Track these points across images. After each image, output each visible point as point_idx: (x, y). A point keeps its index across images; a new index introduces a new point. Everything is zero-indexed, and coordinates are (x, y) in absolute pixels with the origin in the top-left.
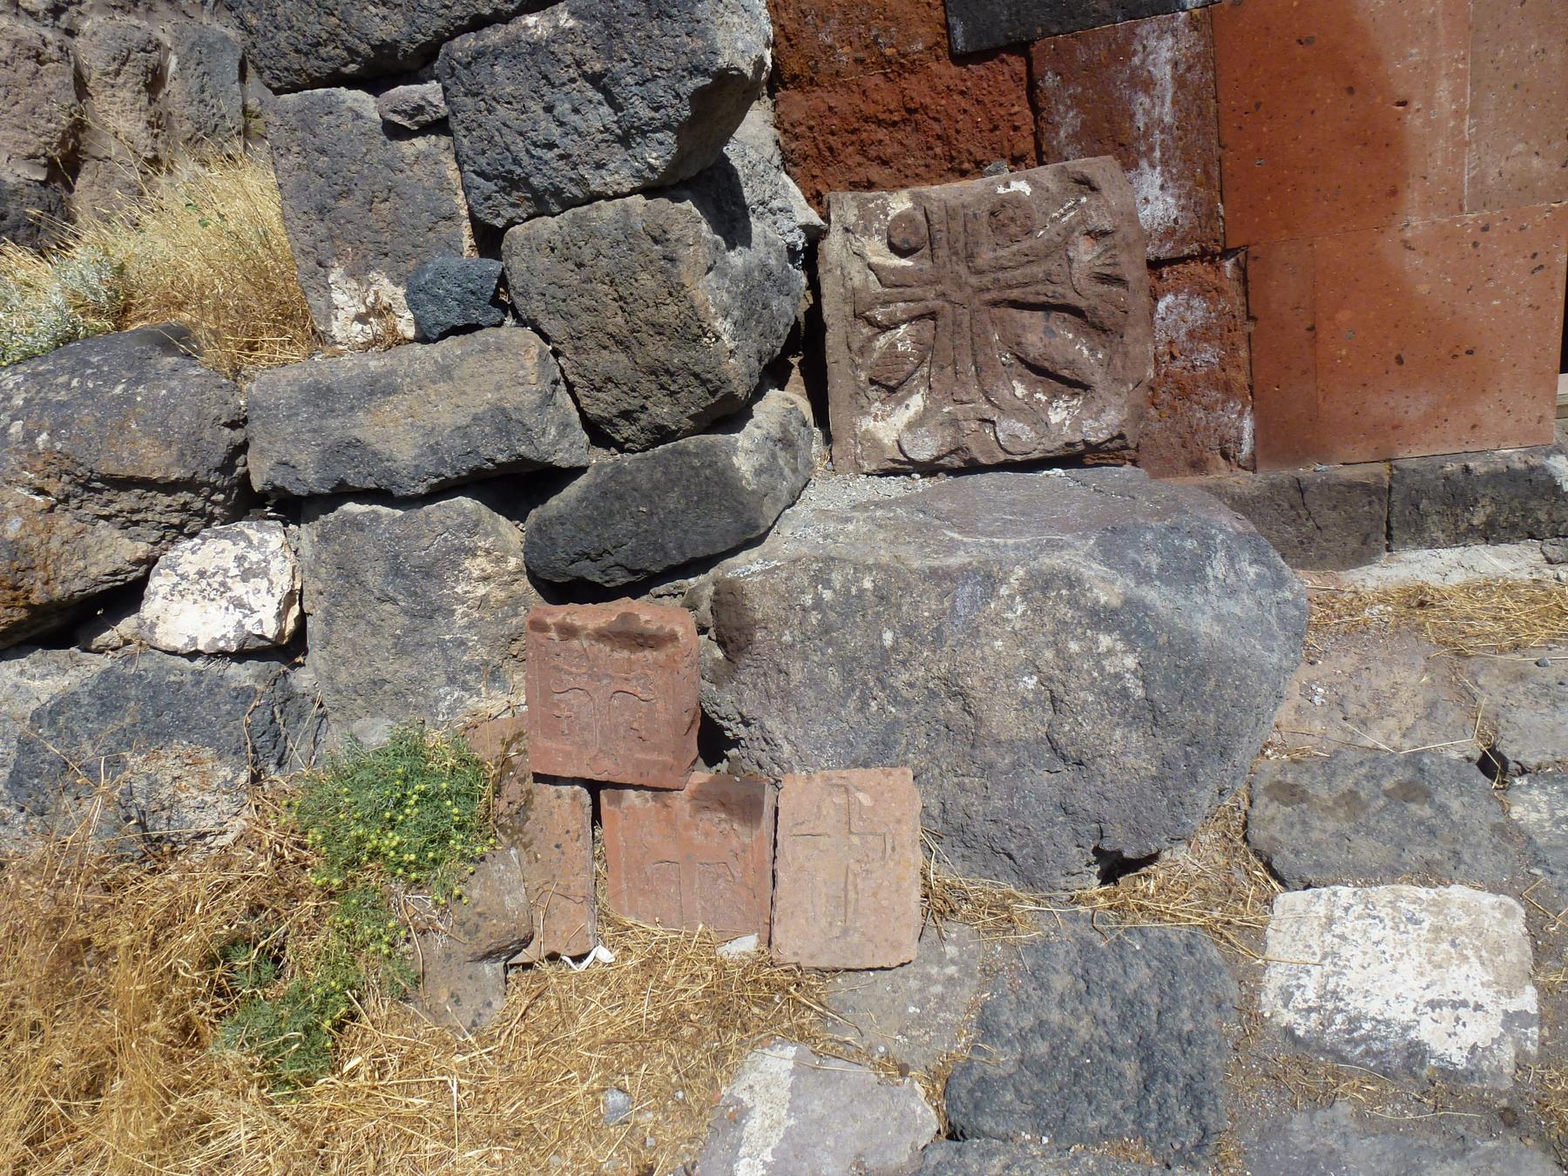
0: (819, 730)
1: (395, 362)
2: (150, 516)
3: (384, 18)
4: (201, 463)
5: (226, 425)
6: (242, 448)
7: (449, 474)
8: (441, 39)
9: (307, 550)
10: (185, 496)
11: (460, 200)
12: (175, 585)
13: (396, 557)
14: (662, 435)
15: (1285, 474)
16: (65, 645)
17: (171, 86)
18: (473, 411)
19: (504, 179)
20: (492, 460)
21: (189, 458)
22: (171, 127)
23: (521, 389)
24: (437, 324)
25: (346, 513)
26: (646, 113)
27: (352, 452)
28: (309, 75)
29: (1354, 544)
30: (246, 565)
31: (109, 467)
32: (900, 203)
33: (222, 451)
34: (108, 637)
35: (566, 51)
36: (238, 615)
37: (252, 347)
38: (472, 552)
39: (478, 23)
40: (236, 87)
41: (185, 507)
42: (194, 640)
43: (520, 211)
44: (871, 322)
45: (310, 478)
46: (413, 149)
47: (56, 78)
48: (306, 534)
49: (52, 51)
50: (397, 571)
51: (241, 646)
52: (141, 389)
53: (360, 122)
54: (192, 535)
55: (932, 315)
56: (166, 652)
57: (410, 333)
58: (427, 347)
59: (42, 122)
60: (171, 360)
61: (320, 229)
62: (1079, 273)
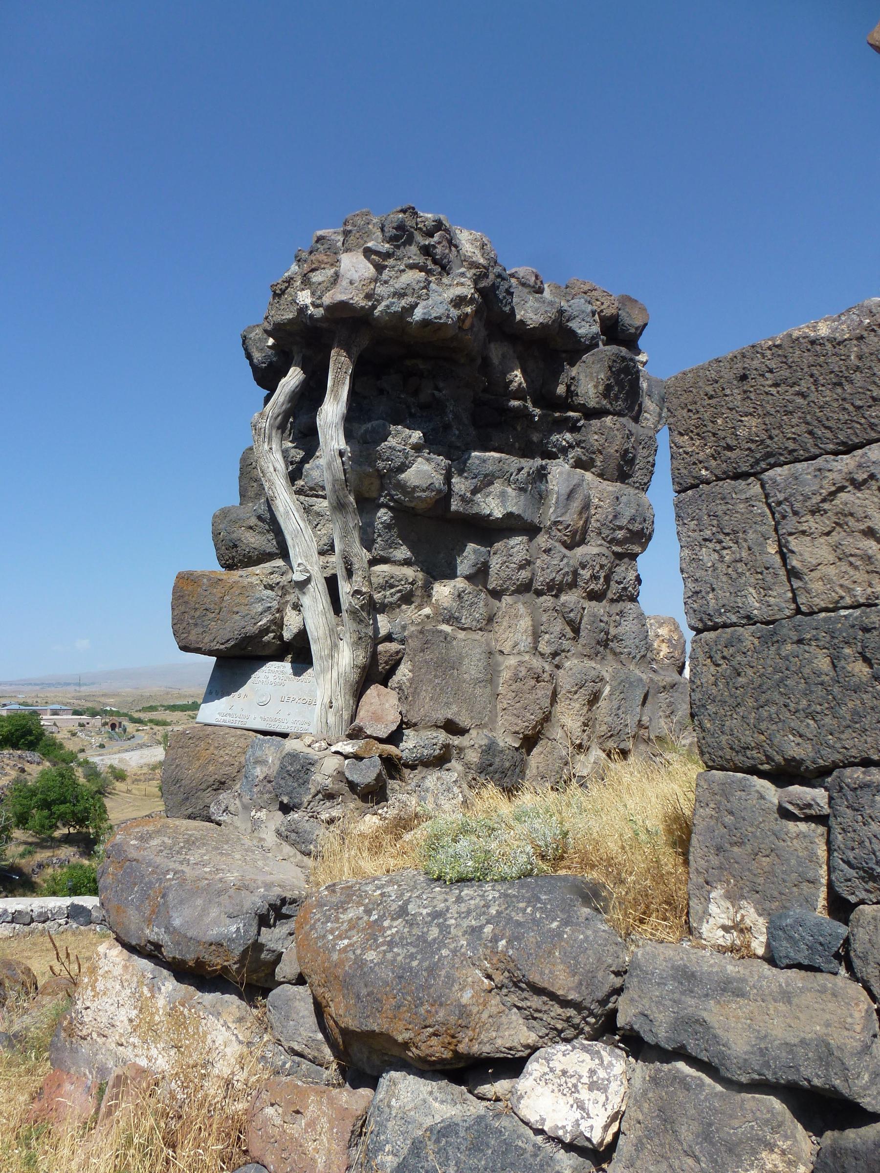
1: (747, 972)
2: (545, 1017)
3: (798, 744)
4: (590, 994)
5: (613, 972)
6: (618, 991)
7: (770, 1077)
8: (835, 766)
9: (637, 1082)
10: (571, 1012)
11: (823, 871)
12: (545, 1074)
13: (710, 1125)
16: (459, 1083)
17: (602, 703)
18: (802, 1035)
19: (865, 871)
20: (809, 1081)
21: (583, 988)
22: (594, 726)
23: (846, 1033)
24: (787, 957)
25: (678, 1070)
27: (698, 1028)
28: (735, 764)
30: (595, 1078)
31: (534, 977)
33: (606, 989)
34: (486, 1089)
36: (578, 1114)
37: (642, 921)
39: (866, 763)
40: (638, 709)
41: (568, 1020)
42: (543, 1120)
43: (872, 896)
45: (660, 1033)
46: (796, 829)
47: (543, 691)
48: (641, 1070)
49: (546, 676)
50: (706, 1136)
51: (573, 1140)
52: (568, 929)
53: (762, 802)
54: (567, 1040)
56: (522, 1121)
57: (760, 951)
58: (774, 970)
59: (528, 714)
60: (586, 911)
61: (715, 861)
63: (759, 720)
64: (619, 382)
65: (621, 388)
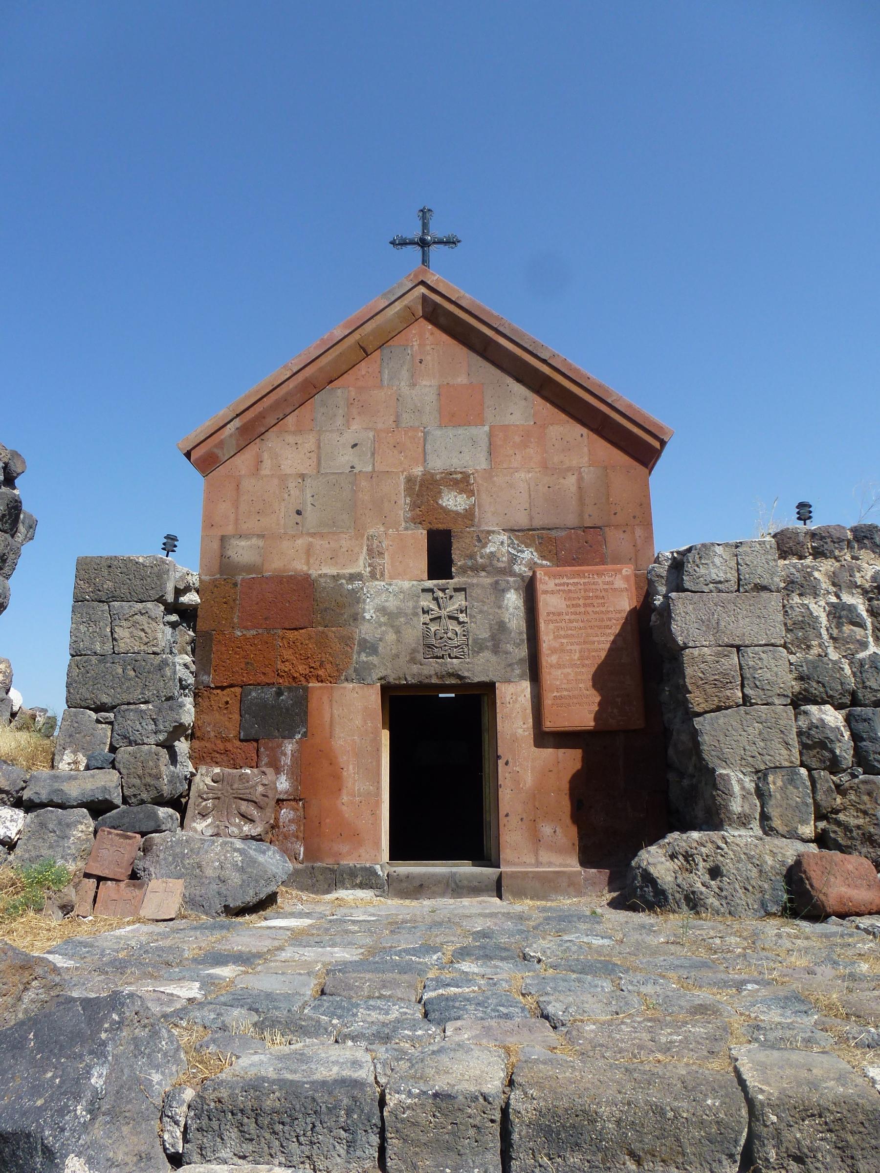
0: (163, 871)
14: (142, 802)
15: (310, 865)
26: (162, 728)
29: (326, 886)
32: (217, 770)
33: (20, 786)
35: (148, 713)
38: (81, 823)
44: (202, 798)
48: (31, 815)
55: (219, 798)
62: (258, 793)
63: (94, 689)
64: (10, 514)
65: (10, 517)
